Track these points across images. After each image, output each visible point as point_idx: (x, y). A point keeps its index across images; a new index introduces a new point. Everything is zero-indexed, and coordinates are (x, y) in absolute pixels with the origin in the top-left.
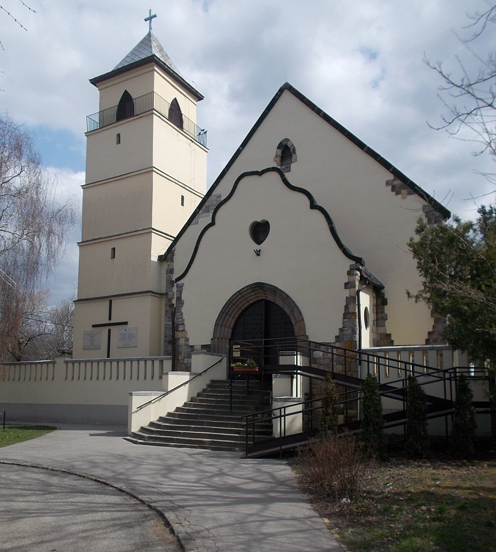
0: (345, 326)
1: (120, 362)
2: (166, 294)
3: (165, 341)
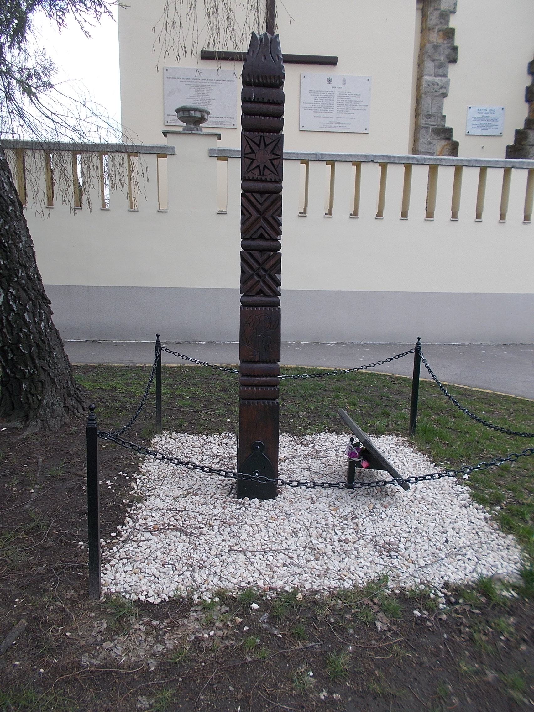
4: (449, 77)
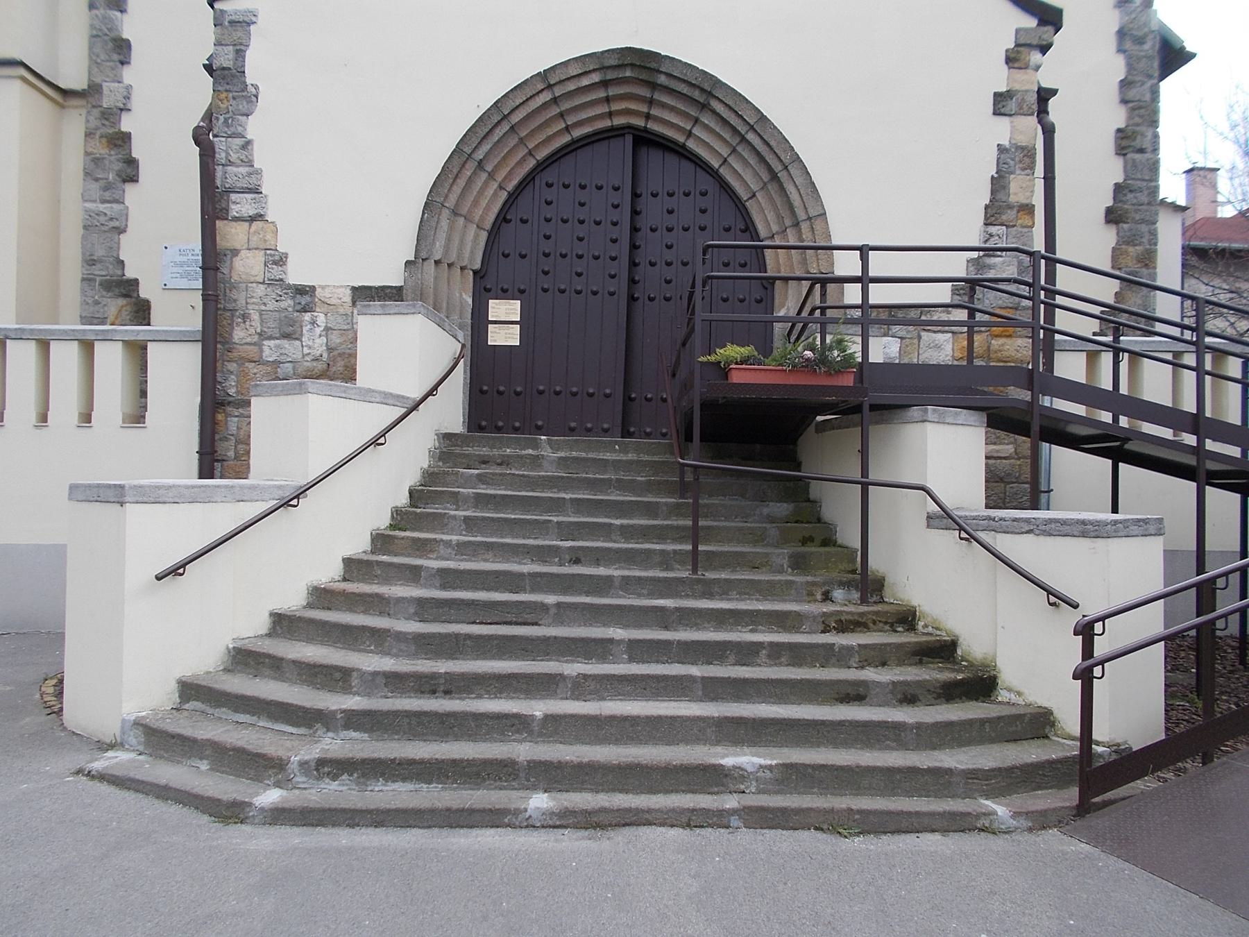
2: (91, 93)
3: (87, 280)
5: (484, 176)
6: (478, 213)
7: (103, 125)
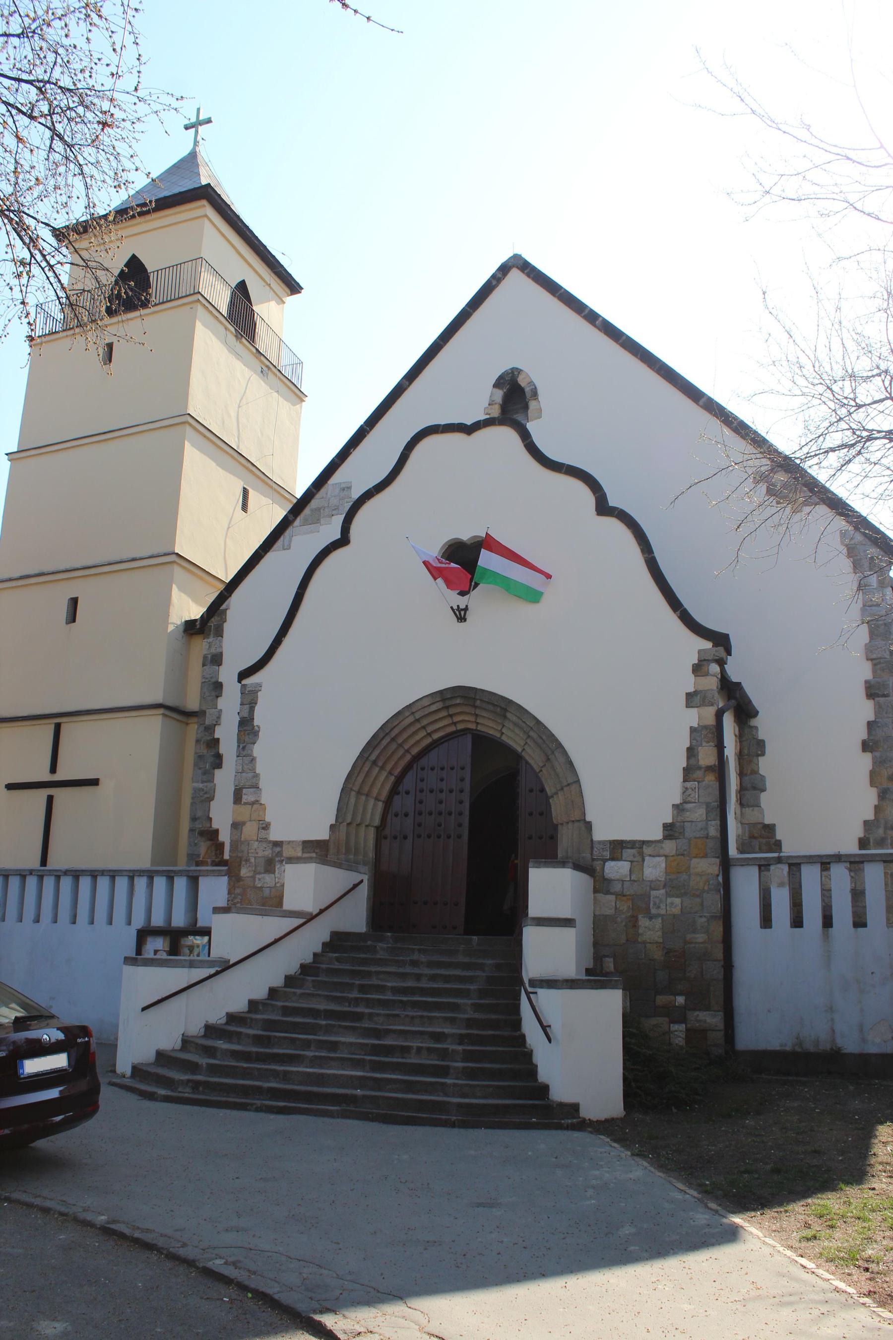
0: (689, 799)
1: (136, 879)
3: (192, 830)
4: (215, 782)
5: (377, 770)
6: (375, 791)
7: (205, 735)
